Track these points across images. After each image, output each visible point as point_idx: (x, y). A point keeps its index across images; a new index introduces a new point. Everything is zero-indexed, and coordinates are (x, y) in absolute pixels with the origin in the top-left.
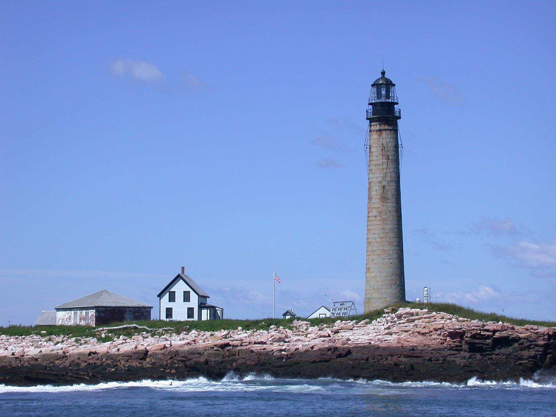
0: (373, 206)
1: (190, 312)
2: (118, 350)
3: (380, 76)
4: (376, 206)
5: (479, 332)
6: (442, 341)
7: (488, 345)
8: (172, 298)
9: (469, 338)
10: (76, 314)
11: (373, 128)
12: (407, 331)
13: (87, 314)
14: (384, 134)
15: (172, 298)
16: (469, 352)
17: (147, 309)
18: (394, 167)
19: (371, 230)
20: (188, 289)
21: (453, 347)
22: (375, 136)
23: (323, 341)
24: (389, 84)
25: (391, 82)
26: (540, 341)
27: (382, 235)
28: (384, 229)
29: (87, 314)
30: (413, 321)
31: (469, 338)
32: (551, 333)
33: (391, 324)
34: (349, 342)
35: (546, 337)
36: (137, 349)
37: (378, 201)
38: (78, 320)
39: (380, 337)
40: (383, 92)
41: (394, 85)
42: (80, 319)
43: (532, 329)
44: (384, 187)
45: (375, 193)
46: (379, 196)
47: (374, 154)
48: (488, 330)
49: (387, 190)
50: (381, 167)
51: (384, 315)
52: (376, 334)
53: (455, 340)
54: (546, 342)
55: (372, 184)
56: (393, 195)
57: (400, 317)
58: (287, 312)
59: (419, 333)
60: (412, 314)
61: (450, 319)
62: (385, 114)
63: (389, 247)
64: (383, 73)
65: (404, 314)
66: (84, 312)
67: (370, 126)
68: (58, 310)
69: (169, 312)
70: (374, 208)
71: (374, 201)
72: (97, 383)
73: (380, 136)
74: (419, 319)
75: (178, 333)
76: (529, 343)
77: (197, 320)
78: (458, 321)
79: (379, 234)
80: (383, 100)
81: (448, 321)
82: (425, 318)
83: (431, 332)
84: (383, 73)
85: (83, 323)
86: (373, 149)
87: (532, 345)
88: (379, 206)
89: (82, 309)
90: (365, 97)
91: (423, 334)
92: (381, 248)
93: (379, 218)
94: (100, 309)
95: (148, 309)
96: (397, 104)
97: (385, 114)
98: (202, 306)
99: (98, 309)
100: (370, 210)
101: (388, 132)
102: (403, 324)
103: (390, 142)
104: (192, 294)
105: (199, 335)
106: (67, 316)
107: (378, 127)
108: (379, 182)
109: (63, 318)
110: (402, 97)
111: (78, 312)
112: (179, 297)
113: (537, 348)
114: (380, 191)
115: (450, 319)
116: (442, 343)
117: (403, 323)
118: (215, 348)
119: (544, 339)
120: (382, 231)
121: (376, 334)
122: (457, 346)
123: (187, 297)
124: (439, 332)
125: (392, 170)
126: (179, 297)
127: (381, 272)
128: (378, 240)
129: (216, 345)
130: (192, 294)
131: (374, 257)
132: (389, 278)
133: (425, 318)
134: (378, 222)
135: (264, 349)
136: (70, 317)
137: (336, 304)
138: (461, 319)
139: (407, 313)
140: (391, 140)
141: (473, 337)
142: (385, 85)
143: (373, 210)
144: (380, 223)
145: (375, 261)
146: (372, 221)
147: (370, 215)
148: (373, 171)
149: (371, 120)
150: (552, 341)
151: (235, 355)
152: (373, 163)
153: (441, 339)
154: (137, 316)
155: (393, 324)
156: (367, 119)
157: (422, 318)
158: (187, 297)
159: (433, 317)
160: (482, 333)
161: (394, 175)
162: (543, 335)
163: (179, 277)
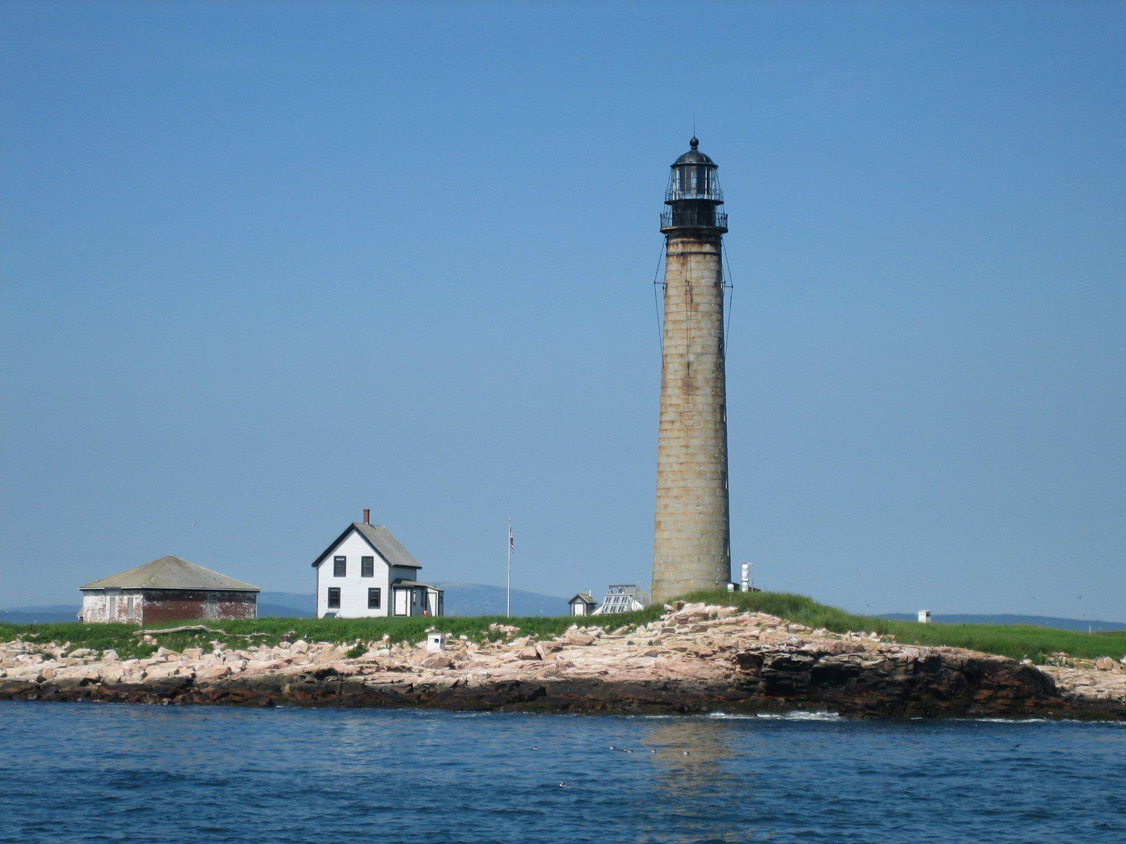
0: (668, 402)
1: (374, 600)
2: (145, 675)
3: (689, 148)
4: (674, 401)
5: (787, 656)
6: (728, 672)
7: (802, 681)
8: (340, 568)
9: (770, 667)
10: (113, 600)
11: (672, 250)
12: (684, 650)
13: (130, 601)
14: (693, 261)
15: (340, 568)
16: (766, 694)
17: (248, 595)
18: (709, 326)
19: (664, 447)
20: (369, 552)
21: (742, 684)
22: (675, 265)
23: (522, 667)
24: (705, 166)
25: (708, 159)
26: (901, 674)
27: (683, 459)
28: (687, 447)
29: (130, 601)
30: (704, 629)
31: (770, 667)
32: (921, 659)
33: (664, 635)
34: (570, 670)
35: (911, 667)
36: (180, 675)
37: (677, 392)
38: (117, 613)
39: (631, 661)
40: (694, 181)
41: (715, 167)
42: (120, 612)
43: (889, 651)
44: (689, 365)
45: (673, 377)
46: (680, 383)
47: (672, 301)
48: (805, 653)
49: (695, 371)
50: (684, 326)
51: (662, 617)
52: (628, 654)
53: (749, 671)
54: (910, 677)
55: (668, 359)
56: (707, 381)
57: (683, 621)
58: (578, 597)
59: (697, 654)
60: (705, 617)
61: (774, 627)
62: (696, 223)
63: (700, 482)
64: (694, 144)
65: (692, 615)
66: (126, 598)
67: (668, 245)
68: (86, 591)
69: (334, 597)
70: (671, 405)
71: (670, 392)
72: (658, 715)
73: (683, 264)
74: (715, 626)
75: (272, 643)
76: (878, 678)
77: (387, 615)
78: (788, 630)
79: (678, 457)
80: (692, 196)
81: (769, 630)
82: (727, 624)
83: (715, 652)
84: (694, 144)
85: (124, 619)
86: (671, 291)
87: (882, 682)
88: (679, 401)
89: (123, 591)
90: (658, 188)
91: (703, 657)
92: (681, 483)
93: (677, 425)
94: (153, 593)
95: (251, 595)
96: (722, 203)
97: (696, 223)
98: (395, 585)
99: (149, 594)
100: (664, 411)
101: (700, 258)
102: (683, 636)
103: (703, 277)
104: (378, 562)
105: (309, 649)
106: (100, 605)
107: (680, 249)
108: (681, 355)
109: (96, 610)
110: (733, 192)
111: (117, 597)
112: (354, 567)
113: (889, 689)
114: (681, 373)
115: (774, 627)
116: (727, 676)
117: (686, 634)
118: (308, 678)
119: (906, 672)
120: (684, 450)
121: (628, 654)
122: (749, 683)
123: (367, 568)
124: (727, 654)
125: (705, 332)
126: (354, 567)
127: (679, 531)
128: (676, 467)
129: (309, 673)
130: (378, 562)
131: (668, 501)
132: (695, 542)
133: (727, 624)
134: (676, 434)
135: (400, 681)
136: (104, 606)
137: (613, 589)
138: (794, 626)
139: (696, 614)
140: (706, 273)
141: (778, 664)
142: (697, 165)
143: (669, 410)
144: (682, 434)
145: (670, 510)
146: (666, 430)
147: (665, 418)
148: (670, 335)
149: (669, 234)
150: (922, 674)
151: (334, 693)
152: (670, 317)
153: (727, 669)
154: (227, 607)
155: (666, 634)
156: (662, 231)
157: (720, 624)
158: (367, 568)
159: (742, 621)
160: (795, 658)
161: (713, 342)
162: (905, 662)
163: (352, 528)
